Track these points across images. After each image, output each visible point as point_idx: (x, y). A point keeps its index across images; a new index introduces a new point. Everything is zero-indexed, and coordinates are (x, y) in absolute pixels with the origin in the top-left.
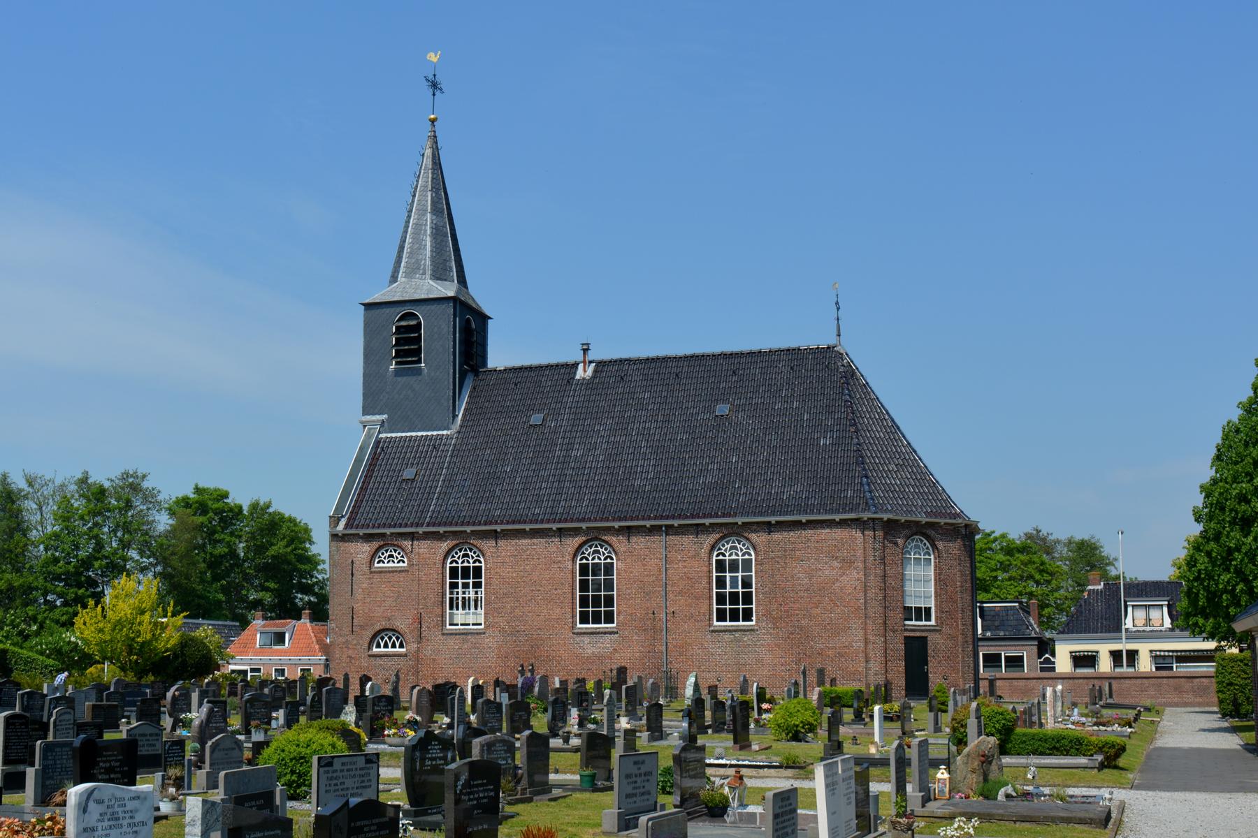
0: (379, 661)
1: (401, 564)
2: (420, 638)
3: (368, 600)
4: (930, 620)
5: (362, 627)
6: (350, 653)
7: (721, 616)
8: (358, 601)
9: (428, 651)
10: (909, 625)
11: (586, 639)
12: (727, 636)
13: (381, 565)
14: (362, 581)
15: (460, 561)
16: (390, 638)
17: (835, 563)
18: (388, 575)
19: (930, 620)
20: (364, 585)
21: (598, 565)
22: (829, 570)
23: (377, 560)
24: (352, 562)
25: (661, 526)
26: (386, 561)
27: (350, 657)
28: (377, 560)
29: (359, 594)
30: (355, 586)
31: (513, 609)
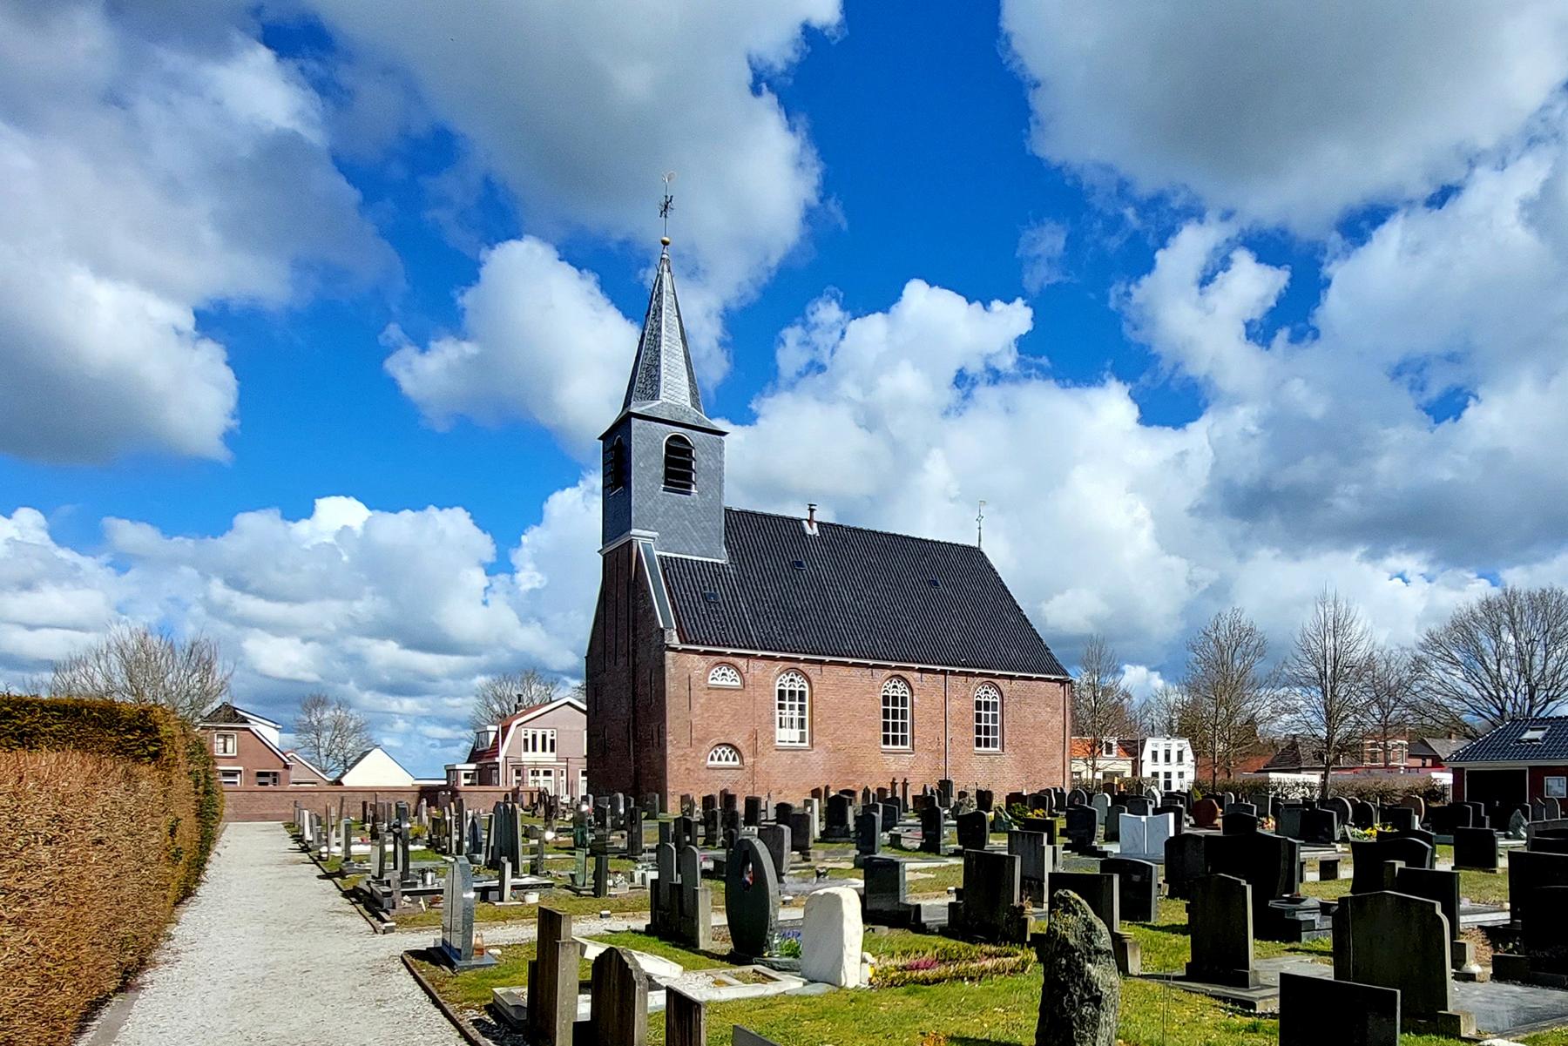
0: (719, 773)
1: (734, 683)
2: (755, 753)
3: (706, 715)
4: (1111, 753)
5: (701, 741)
6: (689, 765)
7: (886, 741)
8: (696, 716)
9: (762, 764)
10: (449, 706)
11: (891, 757)
12: (986, 758)
13: (714, 682)
14: (700, 699)
15: (891, 691)
16: (716, 752)
17: (1049, 709)
18: (725, 692)
19: (1111, 753)
20: (702, 701)
21: (897, 697)
22: (1045, 713)
23: (711, 677)
24: (689, 677)
25: (946, 671)
26: (720, 678)
27: (687, 769)
28: (711, 677)
29: (697, 709)
30: (692, 701)
31: (836, 730)
